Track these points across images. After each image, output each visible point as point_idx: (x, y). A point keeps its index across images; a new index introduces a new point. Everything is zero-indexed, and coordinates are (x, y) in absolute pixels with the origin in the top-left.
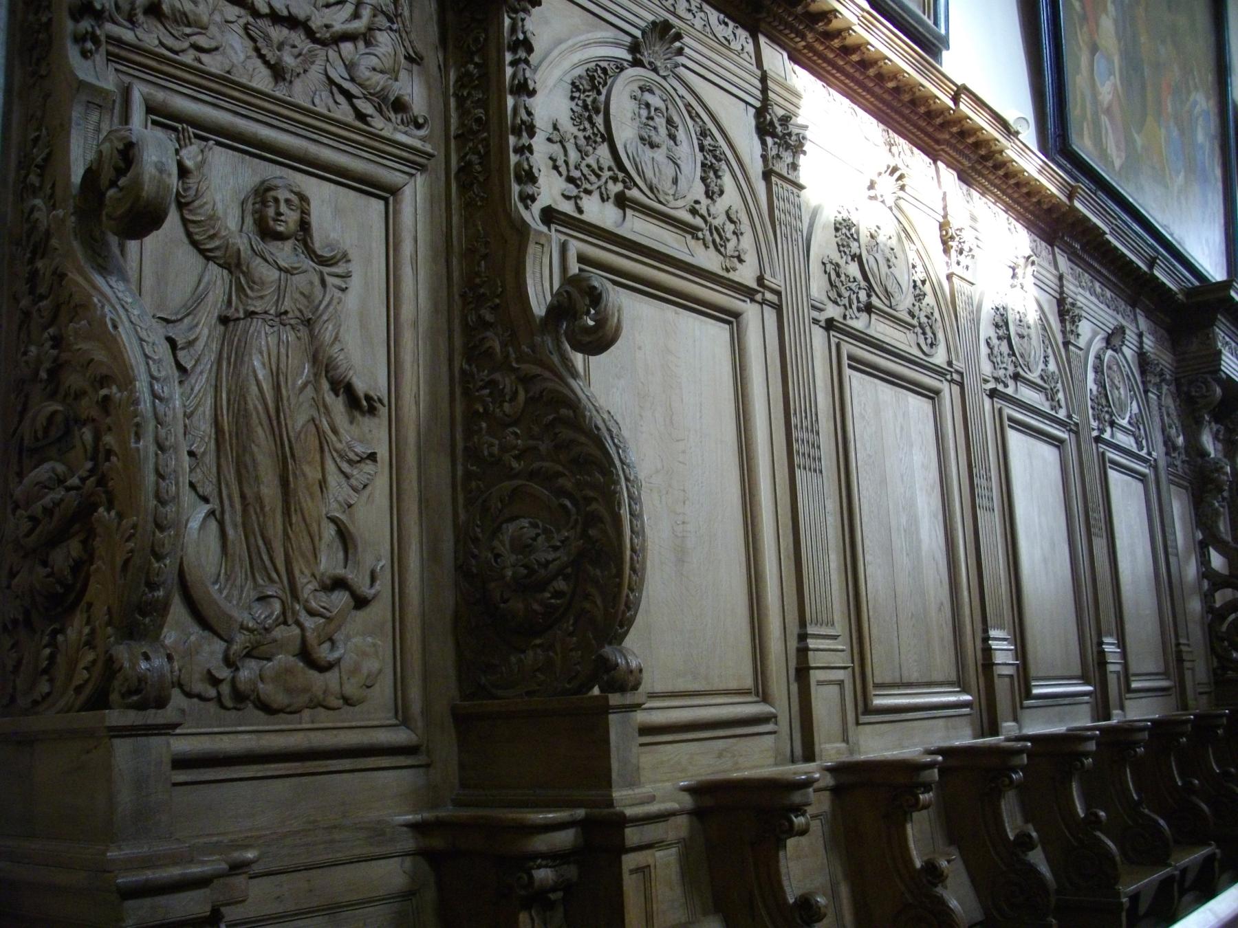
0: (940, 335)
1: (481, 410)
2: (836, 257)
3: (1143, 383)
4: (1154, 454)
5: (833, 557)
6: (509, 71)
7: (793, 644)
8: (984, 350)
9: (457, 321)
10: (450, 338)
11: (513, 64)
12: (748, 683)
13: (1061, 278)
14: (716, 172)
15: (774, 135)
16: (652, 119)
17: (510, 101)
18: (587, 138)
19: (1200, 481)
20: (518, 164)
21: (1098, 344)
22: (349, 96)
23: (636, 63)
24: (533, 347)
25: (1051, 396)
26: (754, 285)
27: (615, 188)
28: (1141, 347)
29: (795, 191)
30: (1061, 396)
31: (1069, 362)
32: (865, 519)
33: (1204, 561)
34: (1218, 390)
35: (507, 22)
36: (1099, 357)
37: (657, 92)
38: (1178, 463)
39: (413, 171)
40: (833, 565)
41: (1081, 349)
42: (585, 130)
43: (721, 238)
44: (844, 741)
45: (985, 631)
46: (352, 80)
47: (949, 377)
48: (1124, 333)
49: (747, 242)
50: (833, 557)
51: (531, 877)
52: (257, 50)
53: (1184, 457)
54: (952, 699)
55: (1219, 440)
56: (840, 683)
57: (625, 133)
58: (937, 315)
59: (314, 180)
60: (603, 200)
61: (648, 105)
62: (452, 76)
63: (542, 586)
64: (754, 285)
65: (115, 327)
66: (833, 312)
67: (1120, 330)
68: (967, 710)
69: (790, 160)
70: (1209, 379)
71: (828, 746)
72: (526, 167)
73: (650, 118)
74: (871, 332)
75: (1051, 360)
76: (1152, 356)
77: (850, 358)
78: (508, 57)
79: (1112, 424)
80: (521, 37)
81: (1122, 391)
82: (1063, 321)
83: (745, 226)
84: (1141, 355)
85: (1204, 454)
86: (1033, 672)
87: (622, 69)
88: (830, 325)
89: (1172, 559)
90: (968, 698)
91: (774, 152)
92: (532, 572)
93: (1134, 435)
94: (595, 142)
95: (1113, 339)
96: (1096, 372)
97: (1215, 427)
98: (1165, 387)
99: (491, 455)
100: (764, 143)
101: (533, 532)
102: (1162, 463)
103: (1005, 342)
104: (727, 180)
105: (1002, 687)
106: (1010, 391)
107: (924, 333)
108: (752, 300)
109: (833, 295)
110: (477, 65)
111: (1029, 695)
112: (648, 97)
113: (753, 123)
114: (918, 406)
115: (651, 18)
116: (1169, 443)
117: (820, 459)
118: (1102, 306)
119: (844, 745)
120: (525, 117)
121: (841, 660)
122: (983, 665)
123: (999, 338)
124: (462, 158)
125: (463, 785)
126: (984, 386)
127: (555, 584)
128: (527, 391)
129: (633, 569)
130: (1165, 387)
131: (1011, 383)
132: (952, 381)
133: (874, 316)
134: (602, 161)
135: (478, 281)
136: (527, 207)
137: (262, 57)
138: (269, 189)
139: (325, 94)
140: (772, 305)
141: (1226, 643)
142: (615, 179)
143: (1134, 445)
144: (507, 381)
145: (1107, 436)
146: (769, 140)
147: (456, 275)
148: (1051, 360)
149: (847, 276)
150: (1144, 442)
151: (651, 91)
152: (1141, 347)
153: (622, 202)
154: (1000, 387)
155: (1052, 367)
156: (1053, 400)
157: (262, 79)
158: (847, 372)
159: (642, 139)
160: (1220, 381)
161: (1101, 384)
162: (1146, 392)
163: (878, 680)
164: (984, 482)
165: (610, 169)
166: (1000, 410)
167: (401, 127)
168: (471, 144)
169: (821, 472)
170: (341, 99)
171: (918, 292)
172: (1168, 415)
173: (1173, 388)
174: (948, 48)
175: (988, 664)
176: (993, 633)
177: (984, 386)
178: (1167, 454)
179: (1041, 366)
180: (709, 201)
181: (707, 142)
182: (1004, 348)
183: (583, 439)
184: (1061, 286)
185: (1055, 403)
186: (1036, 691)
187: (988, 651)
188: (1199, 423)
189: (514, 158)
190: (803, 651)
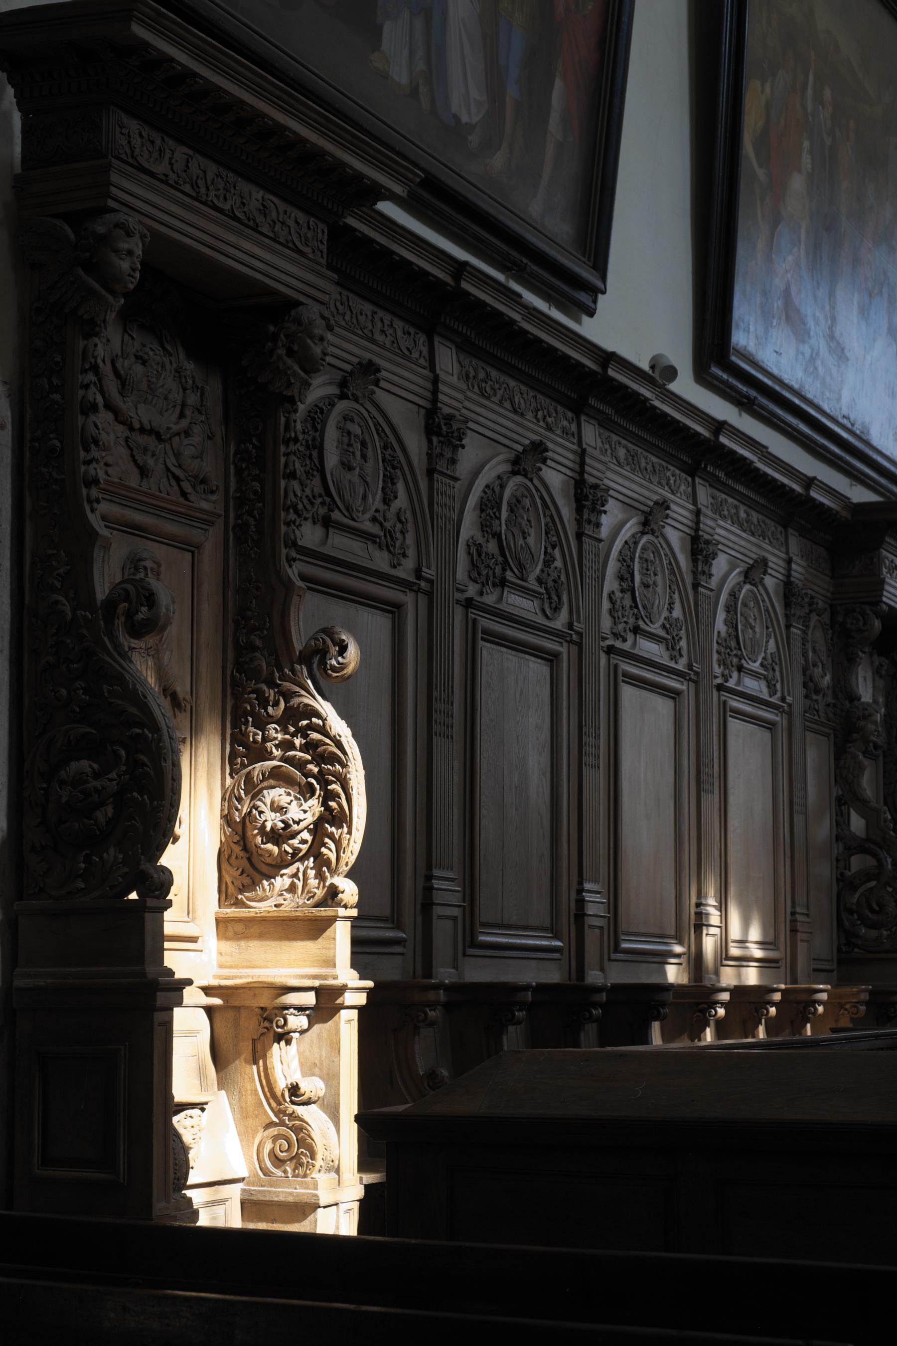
0: (565, 598)
1: (249, 708)
2: (480, 540)
3: (787, 616)
4: (789, 699)
5: (456, 811)
6: (283, 460)
7: (421, 883)
8: (606, 605)
9: (230, 639)
10: (224, 650)
11: (286, 455)
12: (387, 912)
13: (698, 513)
14: (392, 480)
15: (439, 434)
16: (351, 445)
17: (283, 483)
18: (307, 473)
19: (844, 728)
20: (286, 534)
21: (735, 577)
22: (178, 479)
23: (343, 396)
24: (293, 670)
25: (671, 646)
26: (412, 579)
27: (322, 511)
28: (789, 576)
29: (452, 483)
30: (683, 644)
31: (696, 605)
32: (483, 777)
33: (841, 821)
34: (877, 624)
35: (283, 420)
36: (733, 595)
37: (357, 419)
38: (821, 707)
39: (207, 527)
40: (456, 818)
41: (711, 590)
42: (306, 465)
43: (392, 538)
44: (454, 967)
45: (581, 883)
46: (180, 466)
47: (568, 639)
48: (766, 565)
49: (410, 539)
50: (456, 811)
51: (716, 1012)
52: (133, 456)
53: (830, 699)
54: (545, 943)
55: (881, 677)
56: (454, 919)
57: (332, 460)
58: (563, 578)
59: (156, 544)
60: (314, 523)
61: (349, 433)
62: (232, 449)
63: (294, 836)
64: (412, 579)
65: (146, 698)
66: (472, 590)
67: (761, 564)
68: (556, 955)
69: (448, 455)
70: (868, 611)
71: (442, 970)
72: (293, 537)
73: (350, 445)
74: (503, 606)
75: (677, 607)
76: (800, 584)
77: (484, 632)
78: (283, 449)
79: (740, 669)
80: (293, 435)
81: (757, 630)
82: (695, 561)
83: (410, 526)
84: (788, 590)
85: (853, 698)
86: (623, 926)
87: (333, 405)
88: (469, 603)
89: (799, 819)
90: (559, 944)
91: (438, 450)
92: (287, 825)
93: (765, 678)
94: (313, 475)
95: (753, 572)
96: (728, 612)
97: (877, 660)
98: (814, 618)
99: (255, 741)
100: (430, 442)
101: (289, 799)
102: (797, 710)
103: (628, 596)
104: (400, 486)
105: (591, 940)
106: (626, 646)
107: (550, 598)
108: (411, 590)
109: (475, 574)
110: (254, 446)
111: (617, 949)
112: (350, 426)
113: (423, 423)
114: (537, 669)
115: (356, 360)
116: (810, 686)
117: (452, 727)
118: (744, 535)
119: (453, 971)
120: (293, 499)
121: (456, 899)
122: (575, 915)
123: (622, 591)
124: (238, 517)
125: (221, 966)
126: (602, 644)
127: (302, 834)
128: (286, 702)
129: (173, 779)
130: (814, 618)
131: (630, 637)
132: (571, 642)
133: (506, 589)
134: (315, 490)
135: (249, 613)
136: (290, 566)
137: (135, 461)
138: (140, 560)
139: (165, 480)
140: (425, 593)
141: (856, 916)
142: (323, 503)
143: (765, 690)
144: (272, 692)
145: (731, 684)
146: (435, 439)
147: (230, 605)
148: (677, 607)
149: (487, 554)
150: (778, 686)
151: (352, 420)
152: (789, 576)
153: (327, 523)
154: (618, 644)
155: (677, 613)
156: (673, 649)
157: (134, 481)
158: (481, 643)
159: (342, 463)
160: (879, 615)
161: (731, 624)
162: (788, 627)
163: (483, 920)
164: (592, 741)
165: (320, 496)
166: (616, 666)
167: (203, 496)
168: (247, 507)
169: (452, 737)
170: (173, 482)
171: (548, 557)
172: (814, 651)
173: (826, 618)
174: (604, 293)
175: (580, 915)
176: (587, 886)
177: (602, 644)
178: (806, 697)
179: (665, 613)
180: (386, 507)
181: (389, 451)
182: (628, 602)
183: (328, 741)
184: (698, 523)
185: (676, 653)
186: (625, 945)
187: (581, 903)
188: (852, 660)
189: (283, 529)
190: (429, 890)
